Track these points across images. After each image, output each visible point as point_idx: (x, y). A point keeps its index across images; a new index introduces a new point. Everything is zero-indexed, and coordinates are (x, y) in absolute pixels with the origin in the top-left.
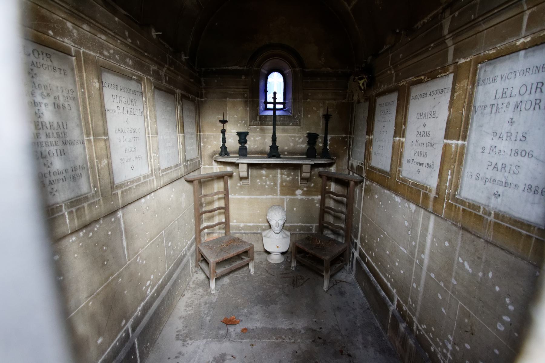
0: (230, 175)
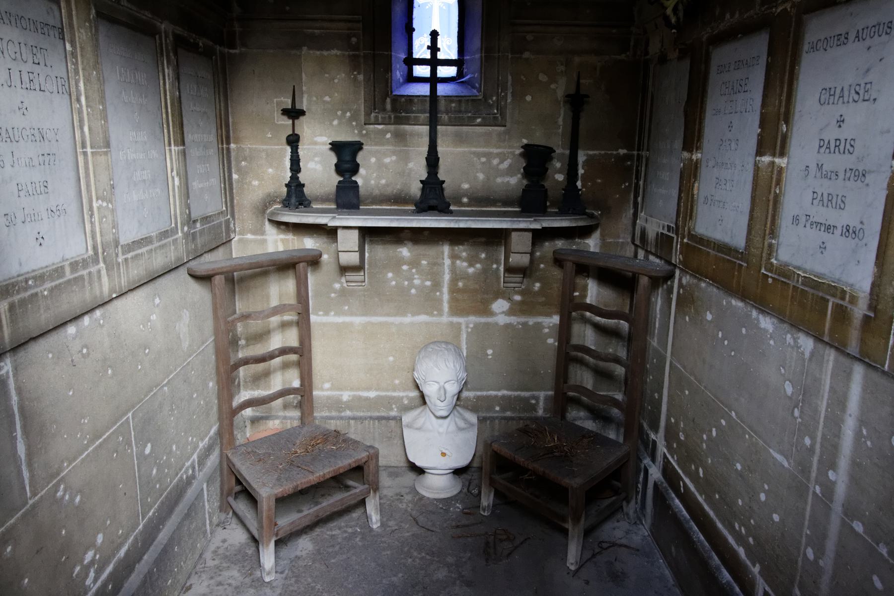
0: (314, 261)
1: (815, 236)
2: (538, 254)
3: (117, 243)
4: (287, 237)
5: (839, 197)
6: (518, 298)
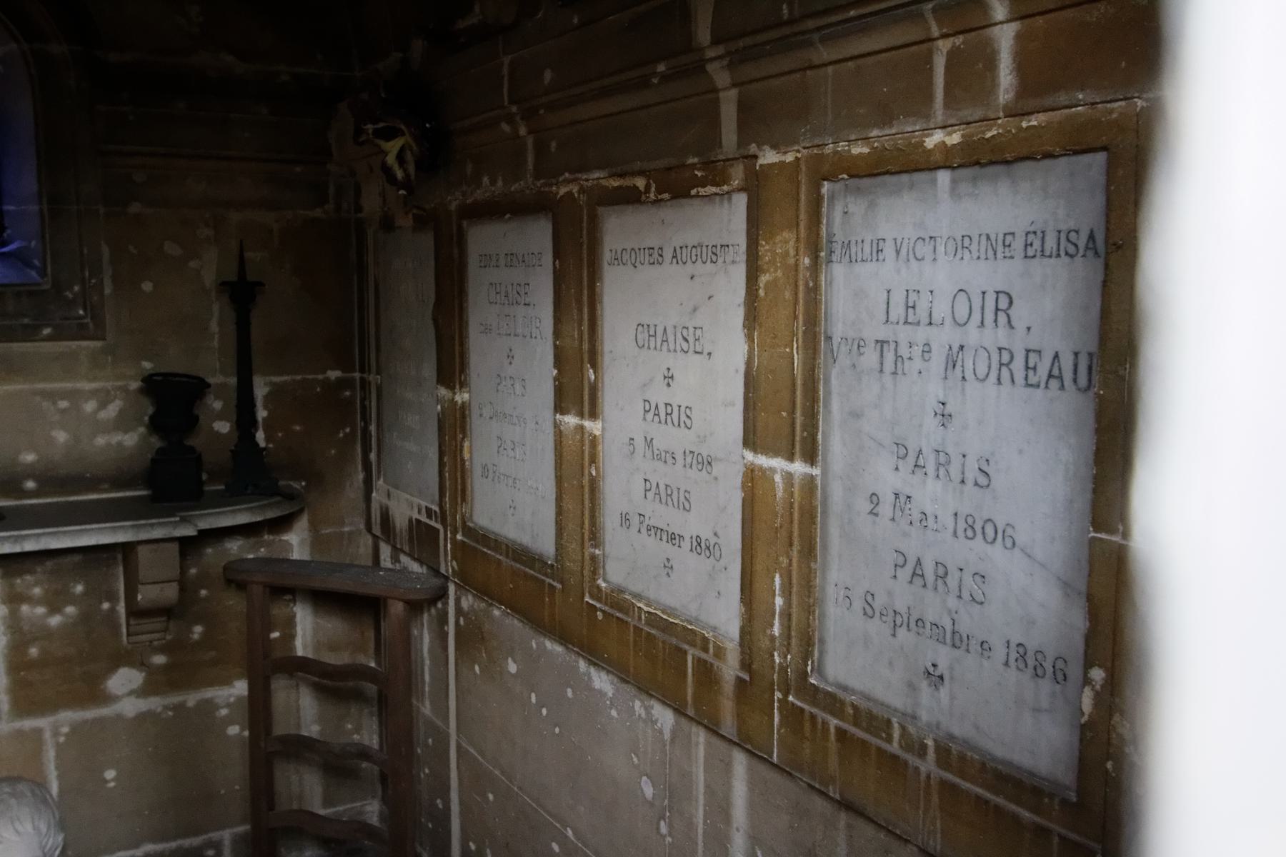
1: (657, 548)
2: (193, 571)
5: (683, 409)
6: (159, 659)
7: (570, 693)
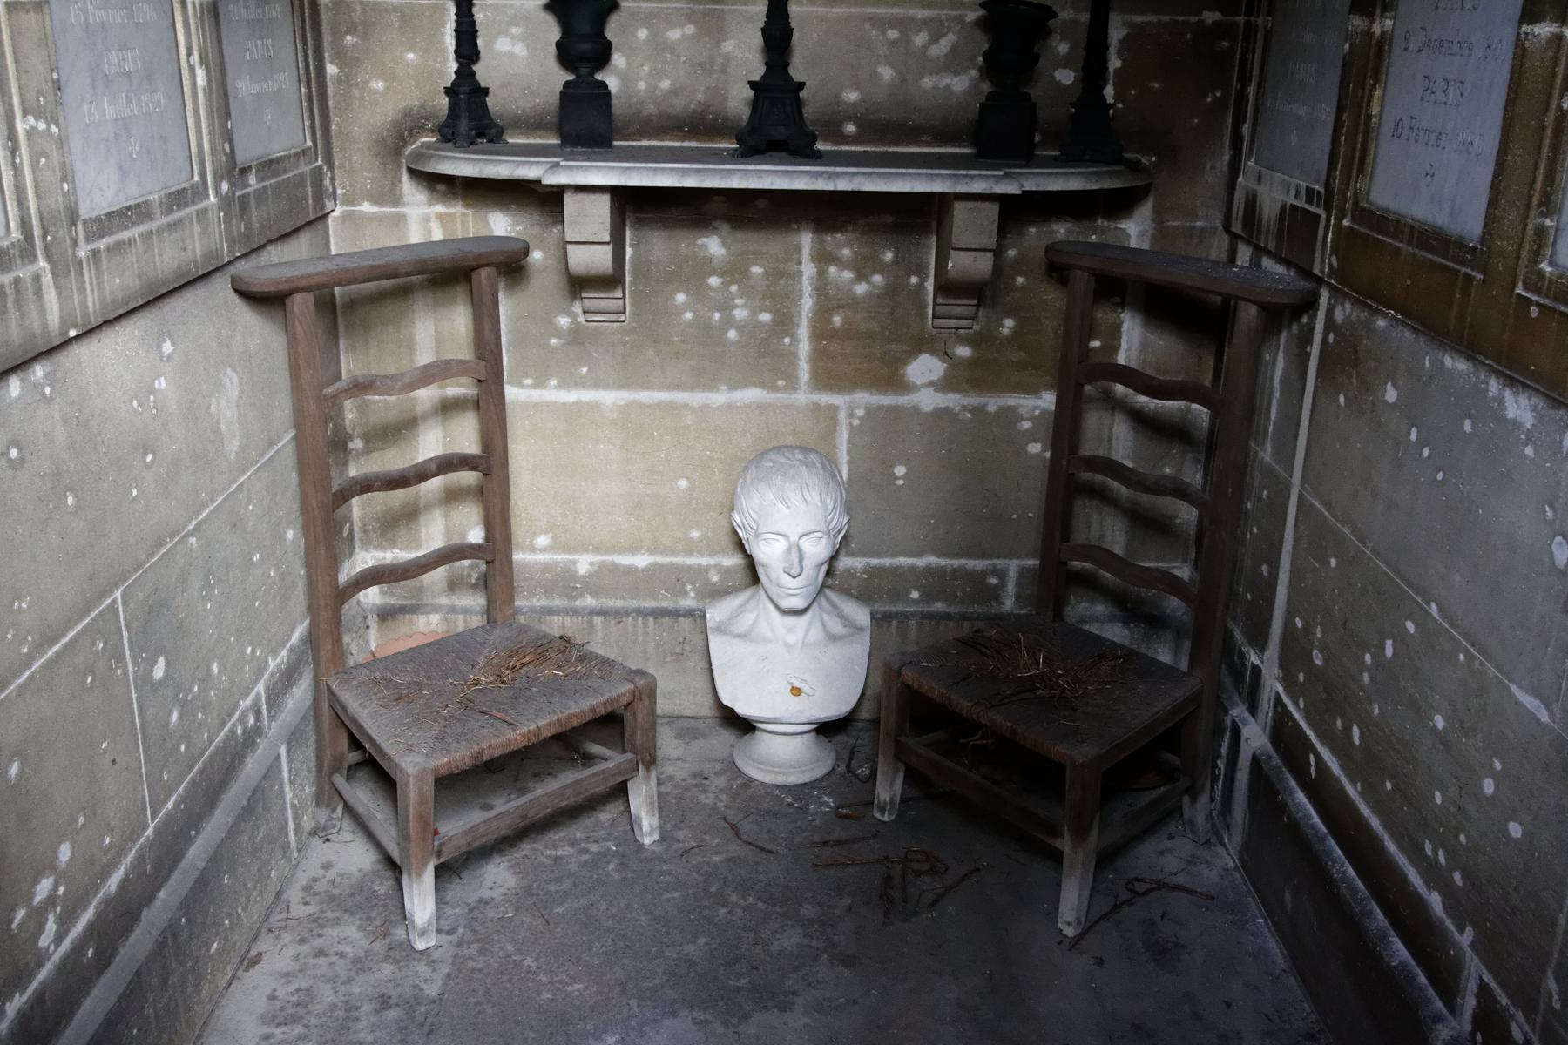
0: (511, 265)
2: (1012, 253)
3: (73, 216)
4: (452, 211)
6: (964, 351)
7: (1467, 426)
